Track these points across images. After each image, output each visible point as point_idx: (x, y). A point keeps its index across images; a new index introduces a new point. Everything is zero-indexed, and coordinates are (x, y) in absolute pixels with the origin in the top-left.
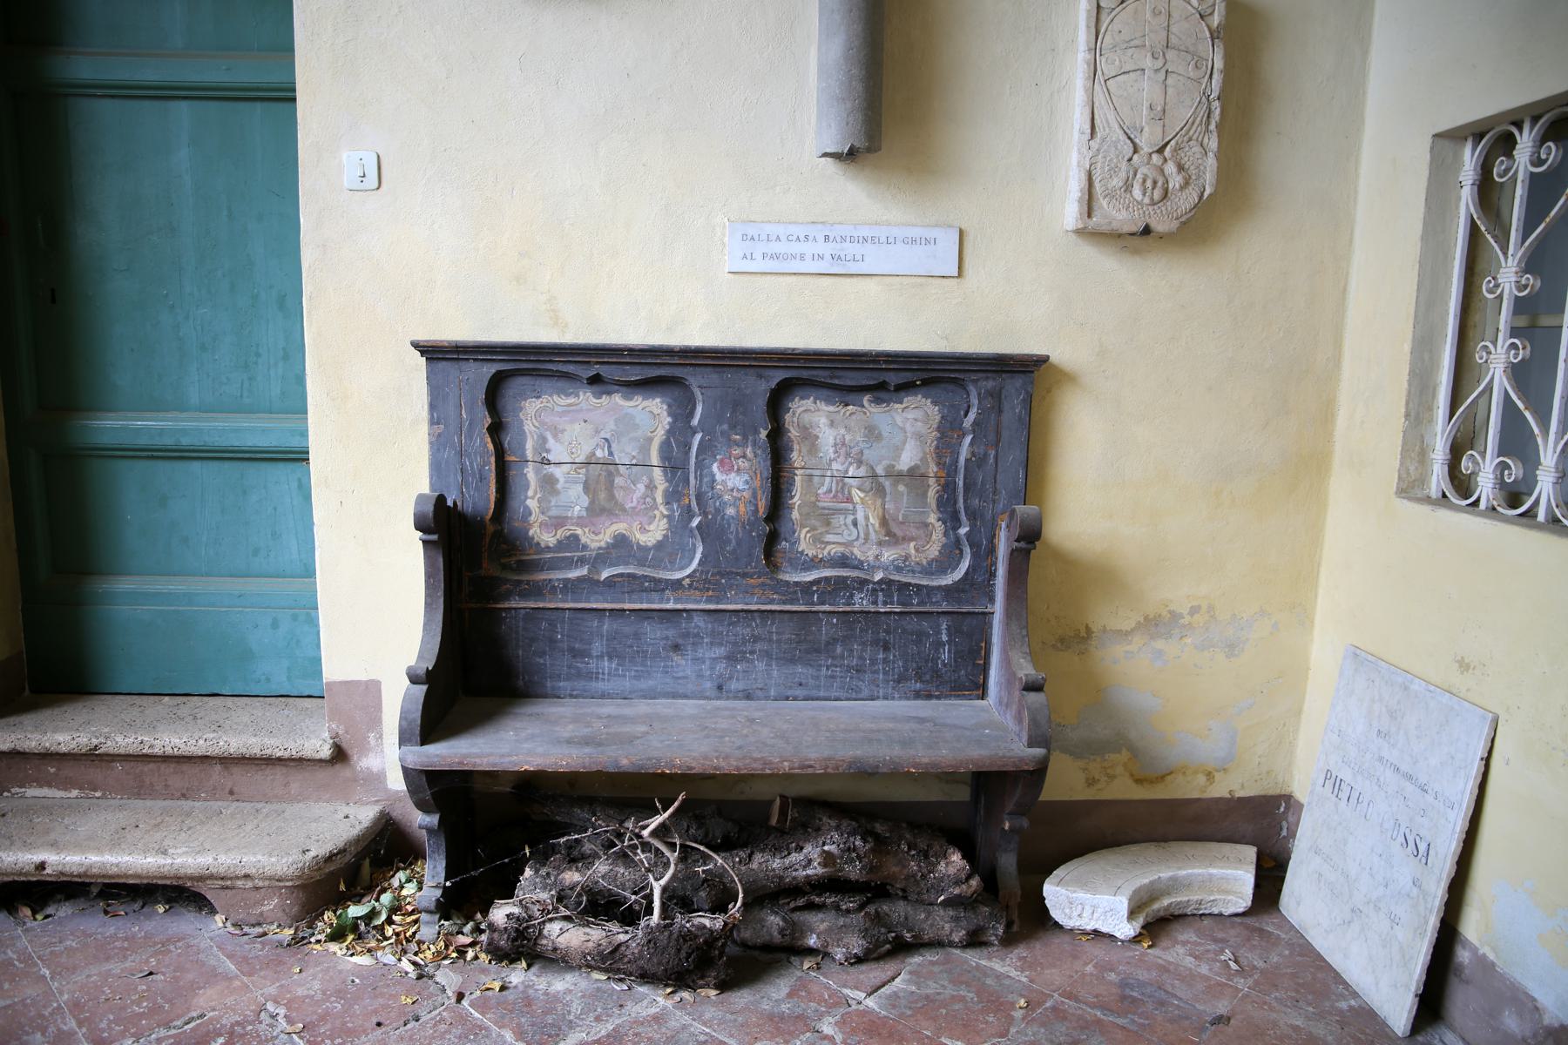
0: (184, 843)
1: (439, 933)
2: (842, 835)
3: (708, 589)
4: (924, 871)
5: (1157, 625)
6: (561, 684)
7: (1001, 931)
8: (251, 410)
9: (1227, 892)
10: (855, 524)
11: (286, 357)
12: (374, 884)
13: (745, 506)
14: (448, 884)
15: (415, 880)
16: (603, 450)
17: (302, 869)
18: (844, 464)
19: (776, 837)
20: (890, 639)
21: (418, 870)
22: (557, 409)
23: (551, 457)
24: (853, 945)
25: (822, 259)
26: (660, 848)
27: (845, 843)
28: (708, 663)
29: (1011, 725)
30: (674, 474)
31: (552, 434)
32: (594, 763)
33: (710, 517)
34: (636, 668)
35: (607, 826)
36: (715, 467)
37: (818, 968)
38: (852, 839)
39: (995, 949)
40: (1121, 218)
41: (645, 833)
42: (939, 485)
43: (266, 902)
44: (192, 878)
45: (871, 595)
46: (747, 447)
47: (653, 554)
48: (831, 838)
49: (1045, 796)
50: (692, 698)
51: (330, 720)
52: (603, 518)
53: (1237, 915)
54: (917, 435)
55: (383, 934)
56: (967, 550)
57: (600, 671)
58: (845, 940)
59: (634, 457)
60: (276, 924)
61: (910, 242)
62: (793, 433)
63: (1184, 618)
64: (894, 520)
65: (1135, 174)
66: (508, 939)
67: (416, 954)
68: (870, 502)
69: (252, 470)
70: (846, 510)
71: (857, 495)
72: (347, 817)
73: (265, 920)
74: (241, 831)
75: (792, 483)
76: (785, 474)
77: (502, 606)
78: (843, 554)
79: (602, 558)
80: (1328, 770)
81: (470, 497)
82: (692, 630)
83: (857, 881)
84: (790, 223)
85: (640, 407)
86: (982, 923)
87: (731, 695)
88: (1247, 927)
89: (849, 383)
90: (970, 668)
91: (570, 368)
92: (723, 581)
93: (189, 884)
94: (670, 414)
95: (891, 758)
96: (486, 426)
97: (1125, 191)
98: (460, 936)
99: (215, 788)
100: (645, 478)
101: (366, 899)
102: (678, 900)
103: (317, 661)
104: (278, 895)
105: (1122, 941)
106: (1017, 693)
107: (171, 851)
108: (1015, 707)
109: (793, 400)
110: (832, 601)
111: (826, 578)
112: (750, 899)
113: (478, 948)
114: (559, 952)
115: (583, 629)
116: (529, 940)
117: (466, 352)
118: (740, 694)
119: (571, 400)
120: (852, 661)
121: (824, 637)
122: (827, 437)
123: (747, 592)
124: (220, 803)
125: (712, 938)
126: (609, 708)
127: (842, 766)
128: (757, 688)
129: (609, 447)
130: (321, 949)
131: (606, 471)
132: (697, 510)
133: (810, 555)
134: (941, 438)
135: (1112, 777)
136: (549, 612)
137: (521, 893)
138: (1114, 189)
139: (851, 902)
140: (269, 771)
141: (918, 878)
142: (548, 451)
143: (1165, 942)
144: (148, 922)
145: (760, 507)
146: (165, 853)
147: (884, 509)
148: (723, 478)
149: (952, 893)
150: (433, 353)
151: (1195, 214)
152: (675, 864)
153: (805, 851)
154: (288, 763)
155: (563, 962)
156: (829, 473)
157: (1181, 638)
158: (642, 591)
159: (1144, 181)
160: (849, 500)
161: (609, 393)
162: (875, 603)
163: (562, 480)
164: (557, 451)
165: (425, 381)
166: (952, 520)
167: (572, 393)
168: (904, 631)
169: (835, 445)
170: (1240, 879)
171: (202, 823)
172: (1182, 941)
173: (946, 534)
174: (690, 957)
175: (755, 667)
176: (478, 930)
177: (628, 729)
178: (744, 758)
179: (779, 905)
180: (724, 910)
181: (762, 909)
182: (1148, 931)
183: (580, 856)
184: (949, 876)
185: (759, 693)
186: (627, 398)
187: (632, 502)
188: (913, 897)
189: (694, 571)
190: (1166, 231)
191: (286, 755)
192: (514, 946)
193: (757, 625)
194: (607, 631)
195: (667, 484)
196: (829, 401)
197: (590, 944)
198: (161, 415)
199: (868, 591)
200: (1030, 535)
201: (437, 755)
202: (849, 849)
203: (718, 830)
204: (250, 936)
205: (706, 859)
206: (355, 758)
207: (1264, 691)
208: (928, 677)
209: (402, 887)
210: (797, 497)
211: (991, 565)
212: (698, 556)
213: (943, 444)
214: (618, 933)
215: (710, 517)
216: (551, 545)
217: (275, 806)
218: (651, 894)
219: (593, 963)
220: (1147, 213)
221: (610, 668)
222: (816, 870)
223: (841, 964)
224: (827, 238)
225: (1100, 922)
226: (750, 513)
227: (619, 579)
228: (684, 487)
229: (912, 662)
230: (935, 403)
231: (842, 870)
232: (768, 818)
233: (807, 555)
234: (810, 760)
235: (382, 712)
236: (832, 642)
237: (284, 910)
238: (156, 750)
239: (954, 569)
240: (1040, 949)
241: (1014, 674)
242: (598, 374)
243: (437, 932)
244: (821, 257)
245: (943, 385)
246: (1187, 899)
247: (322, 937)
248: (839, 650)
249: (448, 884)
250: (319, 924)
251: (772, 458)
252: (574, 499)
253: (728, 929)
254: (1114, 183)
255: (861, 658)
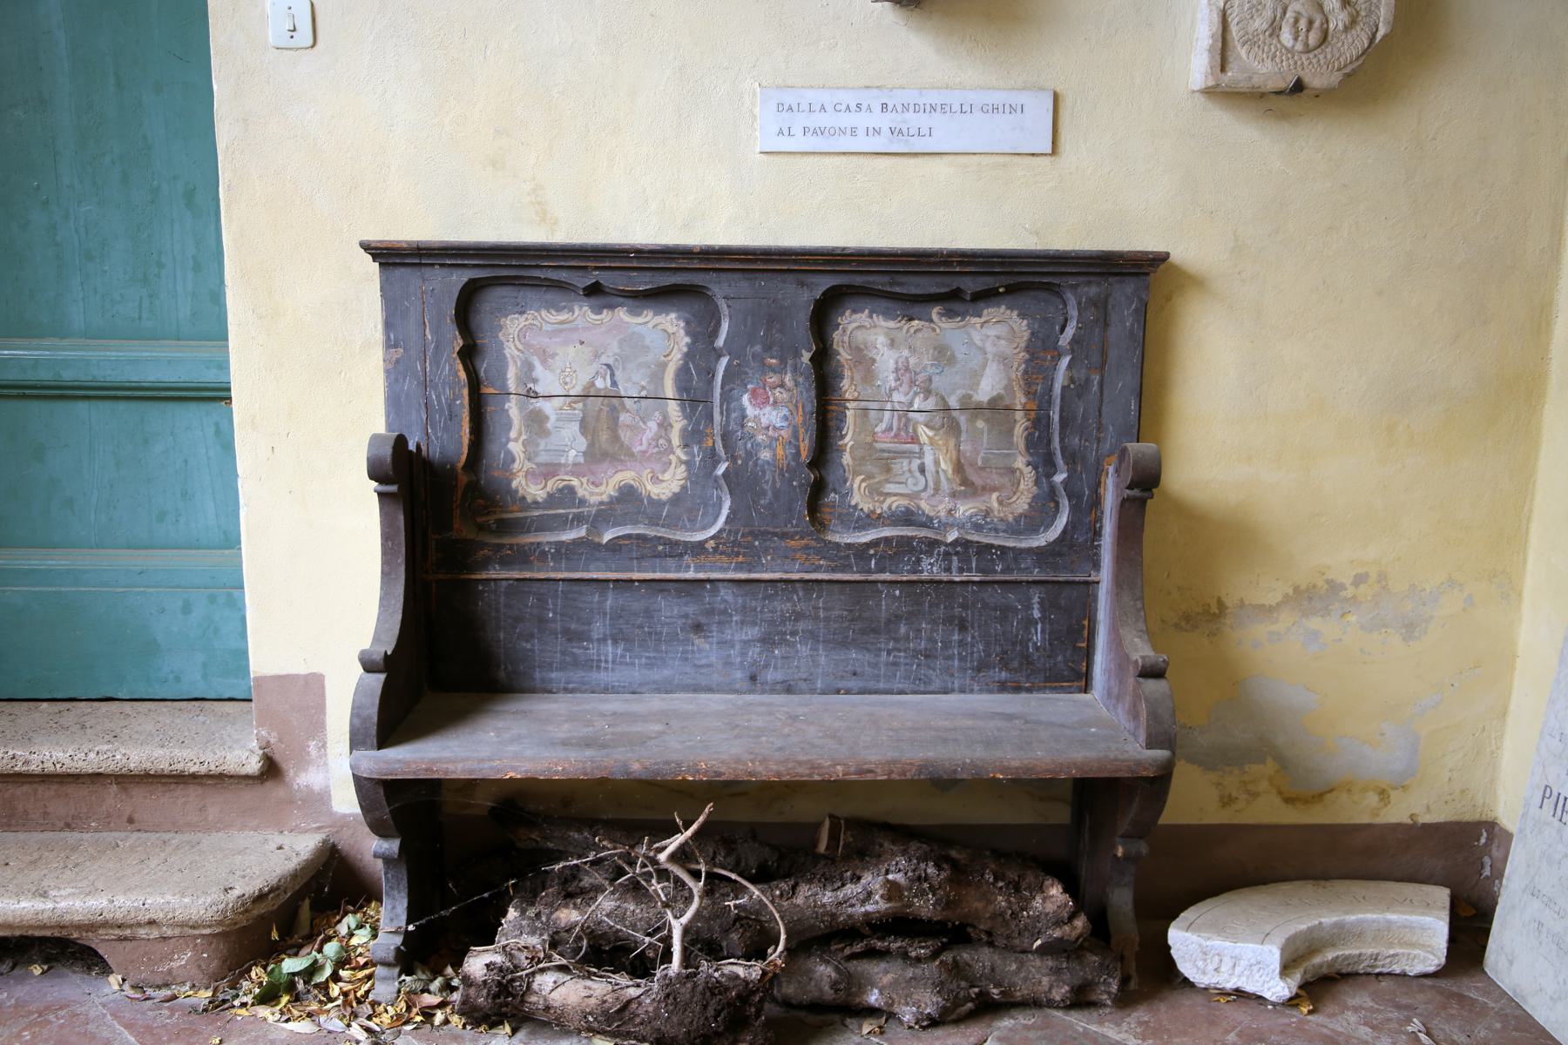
0: (69, 883)
1: (399, 991)
2: (910, 860)
3: (737, 554)
4: (1015, 907)
5: (1310, 599)
6: (553, 675)
7: (1114, 988)
8: (153, 336)
9: (1413, 945)
10: (922, 470)
11: (197, 268)
12: (315, 931)
13: (784, 450)
14: (411, 928)
15: (368, 926)
16: (605, 379)
17: (224, 911)
18: (907, 394)
19: (826, 864)
20: (967, 615)
21: (372, 913)
22: (547, 327)
23: (540, 389)
24: (926, 1004)
25: (879, 134)
26: (681, 876)
27: (914, 871)
28: (738, 647)
29: (1123, 722)
30: (693, 410)
31: (539, 359)
32: (597, 769)
33: (740, 462)
34: (647, 654)
35: (615, 848)
36: (745, 399)
37: (882, 1033)
38: (923, 866)
39: (1108, 1010)
40: (1265, 70)
41: (662, 857)
42: (1029, 420)
43: (176, 957)
44: (79, 927)
45: (944, 560)
46: (786, 373)
47: (668, 511)
48: (897, 864)
49: (1169, 817)
50: (718, 691)
51: (260, 725)
52: (605, 465)
53: (1426, 976)
54: (1000, 357)
55: (327, 995)
56: (1065, 504)
57: (603, 658)
58: (915, 997)
59: (643, 388)
60: (188, 984)
61: (990, 111)
62: (844, 355)
63: (1346, 589)
64: (971, 465)
65: (1284, 13)
66: (488, 995)
67: (369, 1018)
68: (941, 442)
69: (152, 410)
70: (910, 453)
71: (924, 433)
72: (280, 848)
73: (174, 979)
74: (144, 866)
75: (842, 419)
76: (830, 408)
77: (478, 577)
78: (908, 509)
79: (605, 515)
80: (1547, 786)
81: (437, 439)
82: (716, 606)
83: (930, 921)
84: (838, 88)
85: (650, 325)
86: (1090, 977)
87: (767, 688)
88: (1441, 992)
89: (914, 291)
90: (1069, 652)
91: (563, 276)
92: (757, 543)
93: (75, 936)
94: (688, 333)
95: (972, 761)
96: (457, 349)
97: (1270, 35)
98: (426, 995)
99: (109, 815)
100: (657, 414)
101: (304, 951)
102: (702, 944)
103: (244, 654)
104: (191, 946)
105: (1274, 1004)
106: (1131, 681)
107: (52, 893)
108: (1128, 699)
109: (843, 314)
110: (893, 568)
111: (886, 539)
112: (793, 945)
113: (448, 1010)
114: (552, 1011)
115: (580, 605)
116: (514, 997)
117: (430, 256)
118: (778, 687)
119: (564, 316)
120: (920, 644)
121: (883, 614)
122: (886, 360)
123: (786, 557)
124: (114, 834)
125: (747, 991)
126: (614, 704)
127: (910, 771)
128: (801, 679)
129: (612, 375)
130: (247, 1014)
131: (608, 405)
132: (723, 454)
133: (866, 510)
134: (1030, 360)
135: (1254, 795)
136: (539, 584)
137: (504, 939)
138: (1256, 33)
139: (923, 948)
140: (179, 791)
141: (1008, 917)
142: (535, 381)
143: (1330, 1008)
144: (19, 987)
145: (802, 449)
146: (44, 895)
147: (959, 451)
148: (756, 413)
149: (1051, 936)
150: (388, 256)
151: (1363, 64)
152: (700, 897)
153: (863, 881)
154: (204, 781)
155: (557, 1025)
156: (889, 406)
157: (1343, 615)
158: (655, 557)
159: (1296, 21)
160: (915, 439)
161: (612, 307)
162: (948, 570)
163: (553, 418)
164: (547, 382)
165: (379, 293)
166: (1044, 465)
167: (564, 307)
168: (985, 606)
169: (897, 370)
170: (1429, 928)
171: (92, 858)
172: (1353, 1006)
173: (1037, 482)
174: (719, 1015)
175: (798, 651)
176: (448, 988)
177: (639, 729)
178: (787, 760)
179: (830, 952)
180: (761, 955)
181: (809, 957)
182: (1308, 993)
183: (578, 890)
184: (1047, 914)
185: (803, 685)
186: (634, 312)
187: (641, 444)
188: (1000, 942)
189: (720, 531)
190: (1325, 86)
191: (203, 770)
192: (495, 1004)
193: (799, 600)
194: (611, 608)
195: (685, 422)
196: (888, 315)
197: (593, 1001)
198: (35, 342)
199: (939, 554)
200: (1146, 481)
201: (399, 761)
202: (919, 878)
203: (752, 857)
204: (155, 1001)
205: (738, 890)
206: (291, 773)
207: (1456, 685)
208: (1015, 664)
209: (351, 935)
210: (849, 438)
211: (1096, 522)
212: (725, 512)
213: (1034, 368)
214: (628, 987)
215: (740, 462)
216: (540, 500)
217: (187, 837)
218: (670, 937)
219: (595, 1025)
220: (1299, 63)
221: (615, 655)
222: (878, 905)
223: (910, 1028)
224: (884, 107)
225: (1244, 979)
226: (790, 457)
227: (626, 542)
228: (706, 426)
229: (995, 644)
230: (1022, 316)
231: (911, 905)
232: (815, 845)
233: (862, 510)
234: (871, 763)
235: (325, 714)
236: (895, 619)
237: (200, 966)
238: (33, 767)
239: (1048, 527)
240: (1166, 1012)
241: (1127, 657)
242: (597, 282)
243: (396, 990)
244: (877, 132)
245: (1033, 293)
246: (1357, 952)
247: (249, 999)
248: (903, 629)
249: (411, 928)
250: (244, 983)
251: (817, 387)
252: (569, 442)
253: (769, 980)
254: (1257, 24)
255: (931, 640)
